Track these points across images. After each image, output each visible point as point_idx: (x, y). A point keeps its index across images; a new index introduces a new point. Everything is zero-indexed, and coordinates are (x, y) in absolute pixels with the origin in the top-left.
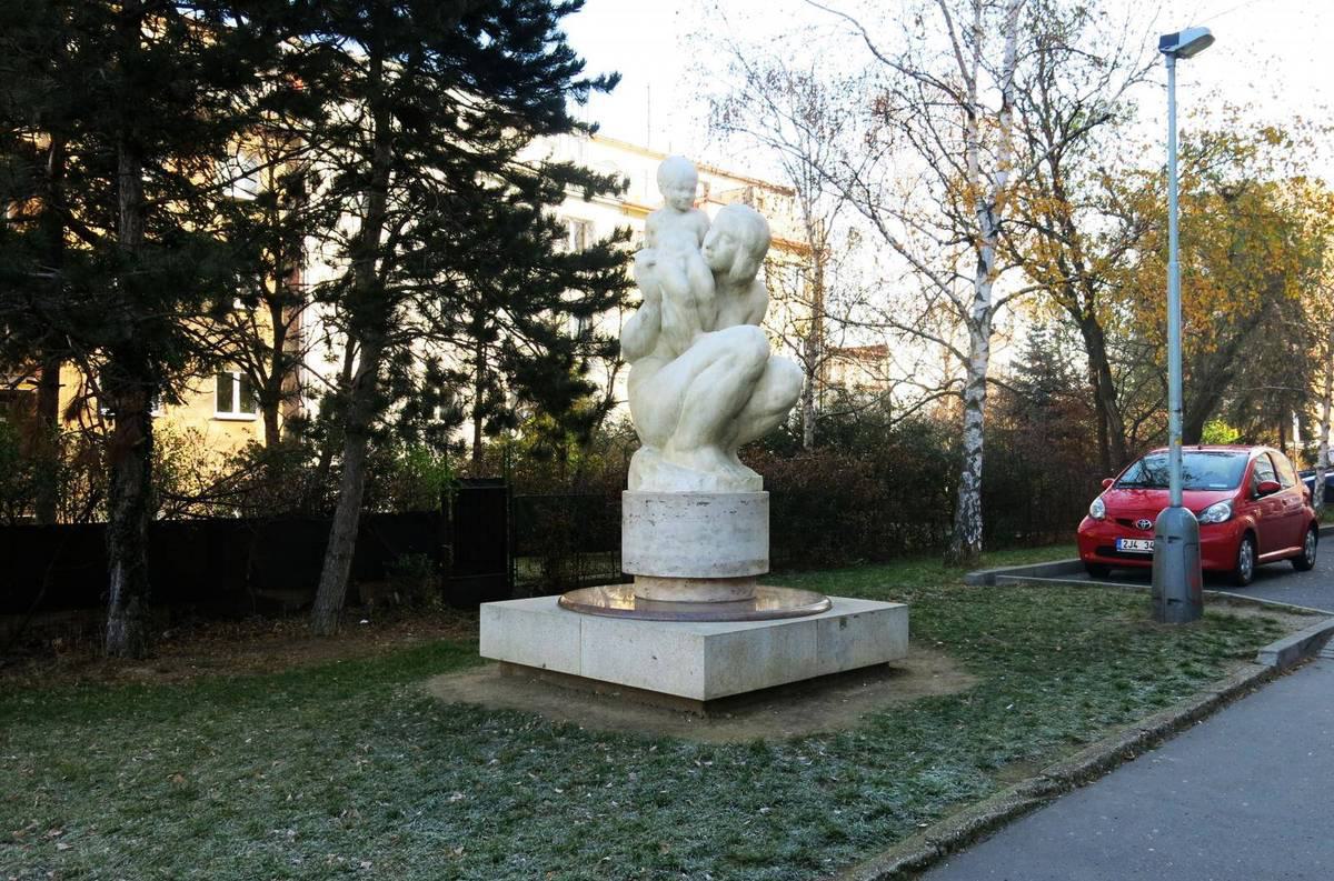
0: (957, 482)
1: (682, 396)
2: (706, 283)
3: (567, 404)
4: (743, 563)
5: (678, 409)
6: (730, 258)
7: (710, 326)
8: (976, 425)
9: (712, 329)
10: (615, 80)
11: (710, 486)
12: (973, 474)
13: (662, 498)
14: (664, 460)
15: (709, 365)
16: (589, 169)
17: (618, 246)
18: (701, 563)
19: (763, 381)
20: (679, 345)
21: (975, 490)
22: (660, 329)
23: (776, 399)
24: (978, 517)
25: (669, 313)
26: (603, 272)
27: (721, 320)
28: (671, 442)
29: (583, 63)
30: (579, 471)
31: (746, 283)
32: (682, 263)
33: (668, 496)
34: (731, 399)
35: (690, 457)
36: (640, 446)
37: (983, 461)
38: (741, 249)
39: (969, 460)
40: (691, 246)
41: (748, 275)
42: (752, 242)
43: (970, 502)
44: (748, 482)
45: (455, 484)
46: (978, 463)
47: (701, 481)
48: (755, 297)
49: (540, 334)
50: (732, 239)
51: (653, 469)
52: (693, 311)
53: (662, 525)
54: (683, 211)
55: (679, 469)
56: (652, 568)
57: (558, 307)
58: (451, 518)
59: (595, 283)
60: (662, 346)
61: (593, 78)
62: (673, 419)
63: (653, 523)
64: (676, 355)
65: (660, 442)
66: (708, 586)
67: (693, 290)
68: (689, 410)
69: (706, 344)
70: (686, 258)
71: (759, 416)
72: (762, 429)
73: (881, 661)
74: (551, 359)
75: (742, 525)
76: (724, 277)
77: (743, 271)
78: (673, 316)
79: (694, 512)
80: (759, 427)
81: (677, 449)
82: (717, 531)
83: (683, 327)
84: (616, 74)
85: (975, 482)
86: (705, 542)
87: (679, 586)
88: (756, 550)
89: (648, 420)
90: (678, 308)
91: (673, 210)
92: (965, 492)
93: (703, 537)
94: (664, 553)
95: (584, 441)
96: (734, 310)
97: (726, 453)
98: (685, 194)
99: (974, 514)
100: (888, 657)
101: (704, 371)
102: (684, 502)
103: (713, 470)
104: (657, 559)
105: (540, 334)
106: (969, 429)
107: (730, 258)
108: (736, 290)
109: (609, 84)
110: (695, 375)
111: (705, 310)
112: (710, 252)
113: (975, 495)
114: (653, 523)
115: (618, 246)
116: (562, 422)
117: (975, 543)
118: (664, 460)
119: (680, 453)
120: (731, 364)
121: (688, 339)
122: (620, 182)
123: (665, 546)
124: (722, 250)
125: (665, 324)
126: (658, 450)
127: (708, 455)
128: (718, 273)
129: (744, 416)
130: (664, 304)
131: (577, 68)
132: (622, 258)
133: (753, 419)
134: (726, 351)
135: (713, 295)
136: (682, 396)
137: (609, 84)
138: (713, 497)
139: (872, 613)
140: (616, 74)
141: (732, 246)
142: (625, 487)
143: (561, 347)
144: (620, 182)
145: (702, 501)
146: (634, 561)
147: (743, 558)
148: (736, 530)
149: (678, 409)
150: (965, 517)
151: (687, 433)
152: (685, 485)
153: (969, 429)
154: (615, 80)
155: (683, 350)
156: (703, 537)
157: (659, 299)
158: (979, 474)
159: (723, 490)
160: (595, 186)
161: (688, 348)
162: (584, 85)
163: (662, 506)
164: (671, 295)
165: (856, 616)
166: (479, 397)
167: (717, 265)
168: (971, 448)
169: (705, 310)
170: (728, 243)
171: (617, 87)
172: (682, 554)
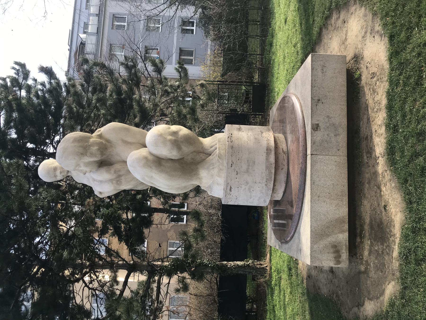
18: (264, 191)
82: (247, 183)
86: (252, 189)
93: (249, 190)
141: (82, 165)
148: (247, 171)
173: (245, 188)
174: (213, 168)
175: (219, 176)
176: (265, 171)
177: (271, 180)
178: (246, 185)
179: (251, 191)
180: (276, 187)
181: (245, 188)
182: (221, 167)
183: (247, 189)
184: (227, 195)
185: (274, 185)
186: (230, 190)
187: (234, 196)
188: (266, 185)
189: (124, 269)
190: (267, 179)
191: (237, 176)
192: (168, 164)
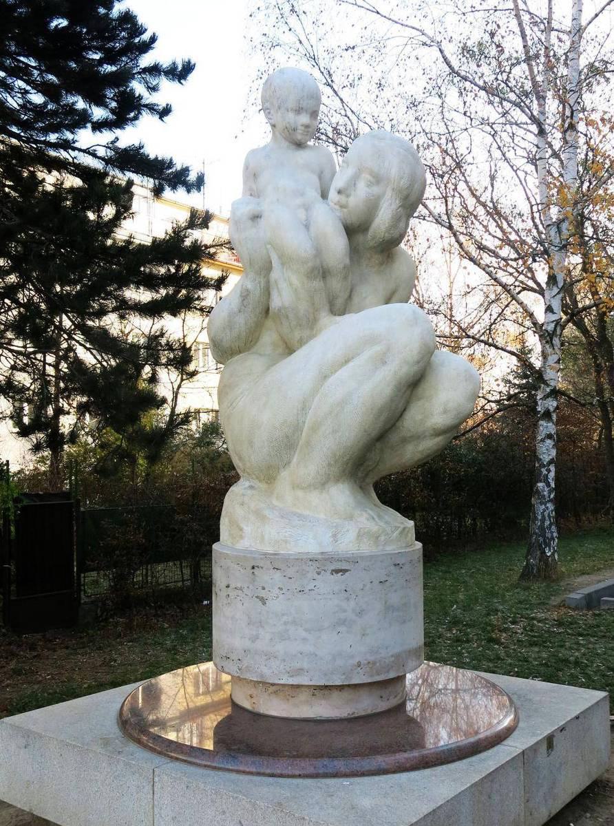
0: (531, 491)
1: (304, 408)
2: (338, 244)
3: (134, 419)
4: (397, 656)
5: (297, 428)
6: (372, 207)
7: (341, 306)
8: (550, 436)
9: (343, 312)
10: (188, 68)
11: (348, 543)
12: (548, 485)
13: (276, 562)
14: (275, 502)
15: (347, 362)
16: (161, 64)
17: (196, 235)
18: (340, 662)
19: (425, 388)
20: (297, 334)
21: (551, 501)
22: (267, 310)
23: (445, 412)
24: (554, 528)
25: (283, 285)
26: (175, 269)
27: (356, 299)
28: (284, 474)
29: (153, 39)
30: (148, 475)
31: (388, 248)
32: (302, 214)
33: (286, 560)
34: (381, 411)
35: (315, 498)
36: (237, 478)
37: (556, 472)
38: (389, 193)
39: (544, 471)
40: (313, 194)
41: (396, 234)
42: (404, 183)
43: (546, 514)
44: (395, 533)
45: (16, 501)
46: (552, 474)
47: (334, 536)
48: (399, 269)
49: (101, 341)
50: (377, 179)
51: (261, 517)
52: (317, 284)
53: (276, 604)
54: (300, 145)
55: (300, 516)
56: (266, 671)
57: (124, 308)
58: (13, 534)
59: (168, 280)
60: (268, 338)
61: (165, 63)
62: (289, 443)
63: (263, 601)
64: (289, 350)
65: (269, 475)
66: (346, 694)
67: (318, 252)
68: (315, 429)
69: (338, 333)
70: (307, 208)
71: (418, 437)
72: (418, 456)
73: (587, 782)
74: (117, 370)
75: (395, 599)
76: (360, 238)
77: (388, 230)
78: (288, 291)
79: (328, 583)
80: (413, 453)
81: (296, 486)
82: (361, 613)
83: (303, 307)
84: (189, 62)
85: (550, 493)
86: (343, 629)
87: (304, 696)
88: (415, 635)
89: (251, 443)
90: (295, 280)
91: (285, 144)
92: (541, 503)
93: (343, 622)
94: (280, 648)
95: (153, 459)
96: (373, 285)
97: (362, 488)
98: (304, 119)
99: (551, 524)
100: (594, 777)
101: (338, 373)
102: (311, 569)
103: (351, 517)
104: (269, 656)
105: (101, 341)
106: (543, 440)
107: (372, 207)
108: (376, 258)
109: (180, 73)
110: (325, 377)
111: (336, 284)
112: (343, 199)
113: (551, 506)
114: (263, 601)
115: (196, 235)
116: (130, 439)
117: (553, 554)
118: (275, 502)
119: (300, 493)
120: (382, 360)
121: (311, 325)
122: (192, 177)
123: (284, 636)
124: (362, 192)
125: (276, 303)
126: (263, 486)
127: (342, 495)
128: (353, 231)
129: (394, 438)
130: (275, 274)
131: (146, 47)
132: (198, 253)
133: (404, 441)
134: (371, 340)
135: (347, 261)
136: (304, 408)
137: (180, 73)
138: (354, 560)
139: (577, 718)
140: (189, 62)
141: (376, 190)
142: (216, 538)
143: (131, 358)
144: (192, 177)
145: (338, 566)
146: (234, 656)
147: (397, 650)
148: (389, 608)
149: (297, 428)
150: (542, 528)
151: (312, 462)
152: (310, 542)
153: (543, 440)
154: (188, 68)
155: (302, 342)
156: (343, 622)
157: (267, 268)
158: (553, 485)
159: (367, 548)
160: (166, 176)
161: (311, 337)
162: (154, 70)
163: (277, 576)
164: (286, 260)
165: (562, 729)
166: (496, 413)
167: (354, 219)
168: (546, 458)
169: (336, 284)
170: (370, 184)
171: (191, 77)
172: (308, 648)
173: (345, 611)
174: (373, 518)
175: (360, 536)
176: (391, 654)
177: (372, 676)
178: (354, 610)
179: (340, 629)
180: (336, 694)
181: (345, 611)
182: (382, 538)
183: (342, 616)
184: (316, 564)
185: (341, 688)
186: (337, 571)
187: (315, 583)
188: (359, 665)
189: (229, 294)
190: (374, 663)
191: (376, 582)
192: (401, 406)
